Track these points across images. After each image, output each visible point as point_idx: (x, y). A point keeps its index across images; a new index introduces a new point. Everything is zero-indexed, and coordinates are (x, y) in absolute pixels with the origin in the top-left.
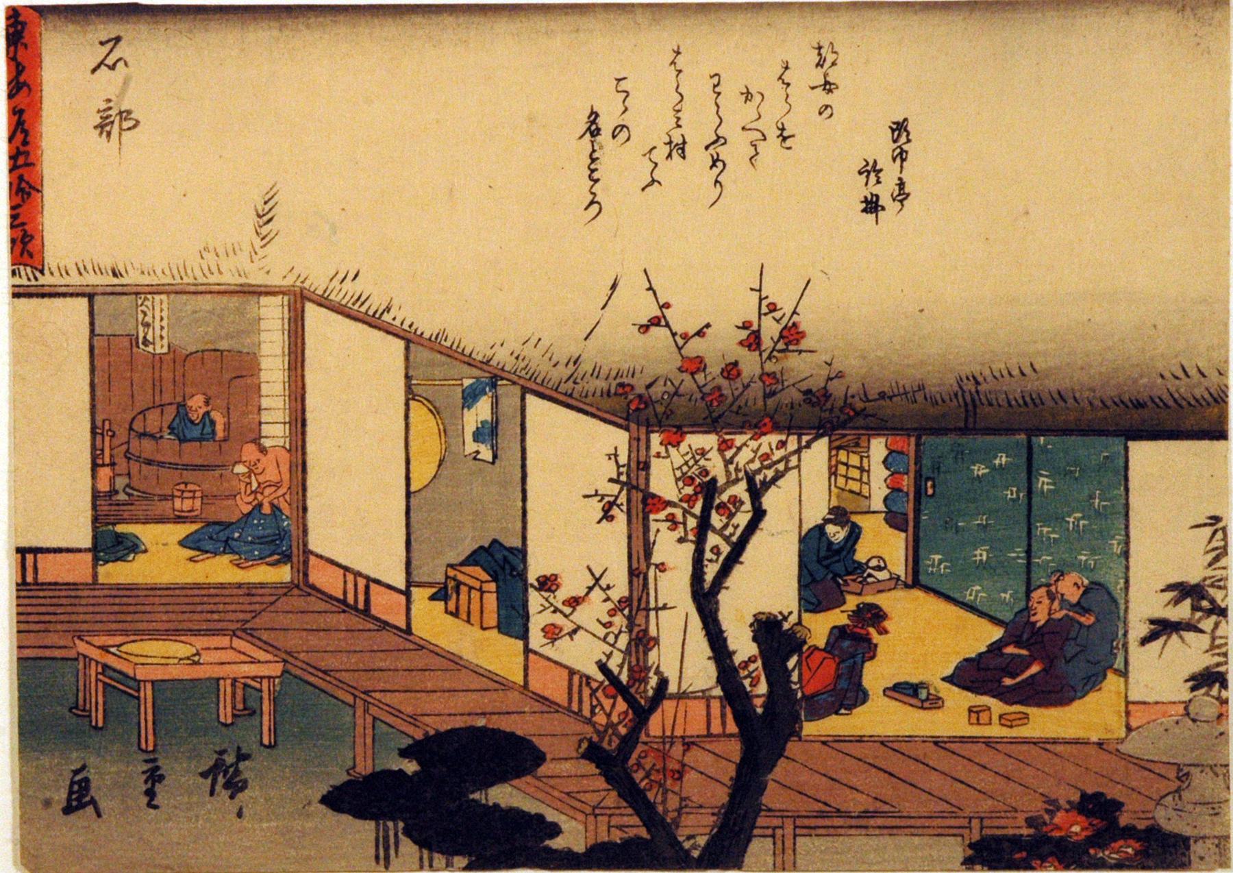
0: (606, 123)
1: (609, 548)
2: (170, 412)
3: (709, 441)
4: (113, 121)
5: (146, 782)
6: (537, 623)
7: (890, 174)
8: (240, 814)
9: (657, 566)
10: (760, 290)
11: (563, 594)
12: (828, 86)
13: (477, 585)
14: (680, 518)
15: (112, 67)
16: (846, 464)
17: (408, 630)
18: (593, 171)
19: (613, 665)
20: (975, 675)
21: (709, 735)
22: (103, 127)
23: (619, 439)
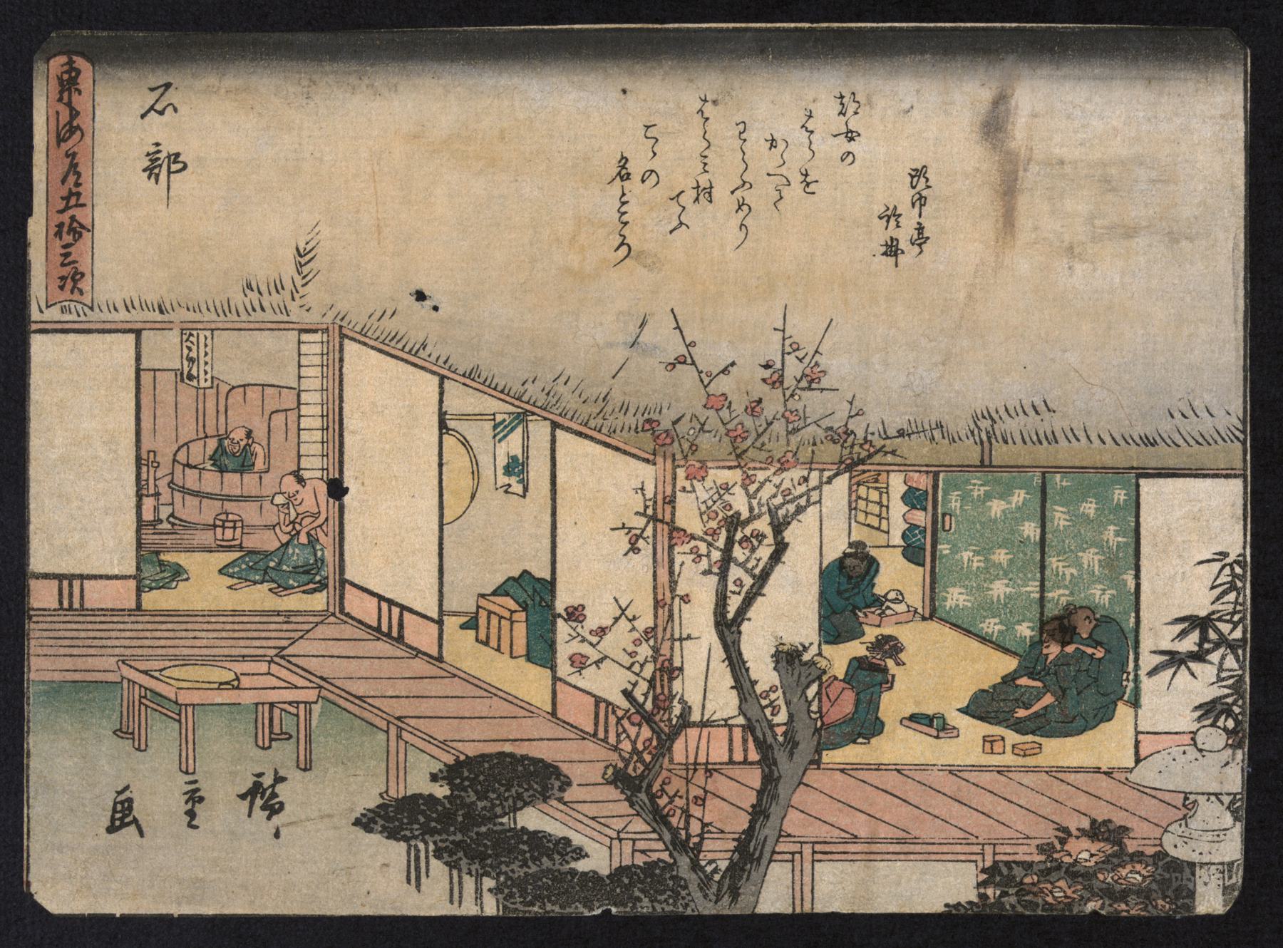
0: (635, 168)
2: (212, 444)
4: (162, 165)
6: (564, 650)
7: (909, 221)
9: (682, 598)
12: (850, 136)
13: (507, 614)
15: (161, 113)
16: (866, 499)
17: (440, 659)
22: (151, 171)
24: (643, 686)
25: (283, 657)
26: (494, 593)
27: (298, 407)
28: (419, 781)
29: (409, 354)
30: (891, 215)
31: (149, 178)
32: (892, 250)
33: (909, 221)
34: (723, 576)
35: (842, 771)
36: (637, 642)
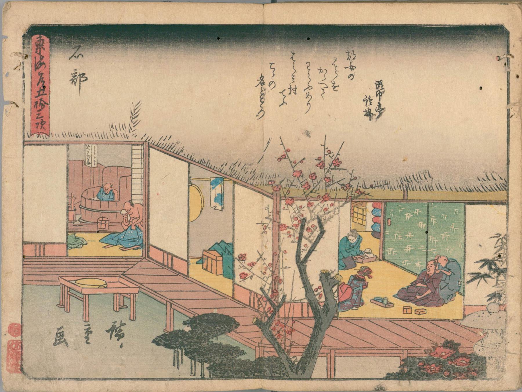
0: (267, 81)
4: (77, 78)
6: (238, 271)
7: (375, 100)
10: (324, 146)
18: (262, 99)
21: (303, 317)
22: (73, 81)
27: (131, 175)
28: (179, 325)
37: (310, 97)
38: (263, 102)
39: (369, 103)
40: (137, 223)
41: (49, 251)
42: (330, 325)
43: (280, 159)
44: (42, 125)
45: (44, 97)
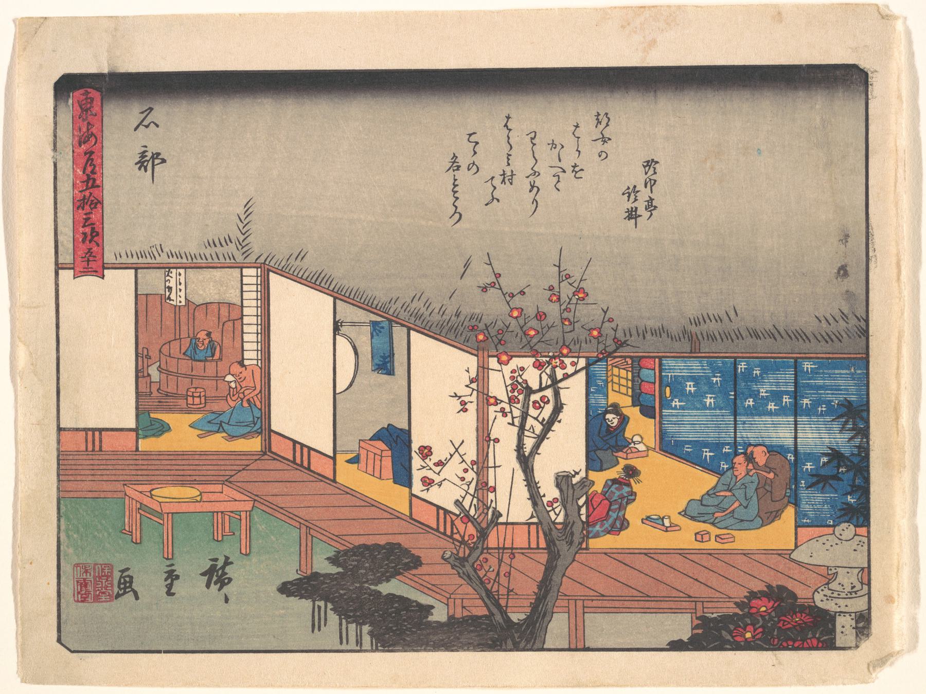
0: (464, 161)
1: (465, 427)
2: (186, 343)
3: (528, 362)
4: (148, 161)
5: (166, 580)
6: (417, 476)
7: (644, 194)
8: (227, 600)
9: (494, 440)
10: (559, 267)
11: (435, 458)
12: (605, 140)
13: (379, 452)
14: (508, 409)
15: (147, 127)
16: (619, 376)
17: (334, 481)
18: (455, 192)
19: (466, 504)
20: (697, 511)
21: (530, 548)
22: (141, 164)
23: (471, 362)
24: (469, 498)
25: (230, 482)
26: (370, 440)
27: (242, 318)
28: (322, 566)
29: (316, 282)
30: (630, 193)
31: (140, 168)
32: (632, 215)
33: (644, 194)
34: (522, 428)
35: (605, 554)
36: (466, 471)
37: (535, 189)
38: (457, 198)
39: (632, 197)
40: (251, 395)
41: (108, 442)
42: (574, 560)
43: (484, 289)
44: (93, 237)
45: (96, 192)
